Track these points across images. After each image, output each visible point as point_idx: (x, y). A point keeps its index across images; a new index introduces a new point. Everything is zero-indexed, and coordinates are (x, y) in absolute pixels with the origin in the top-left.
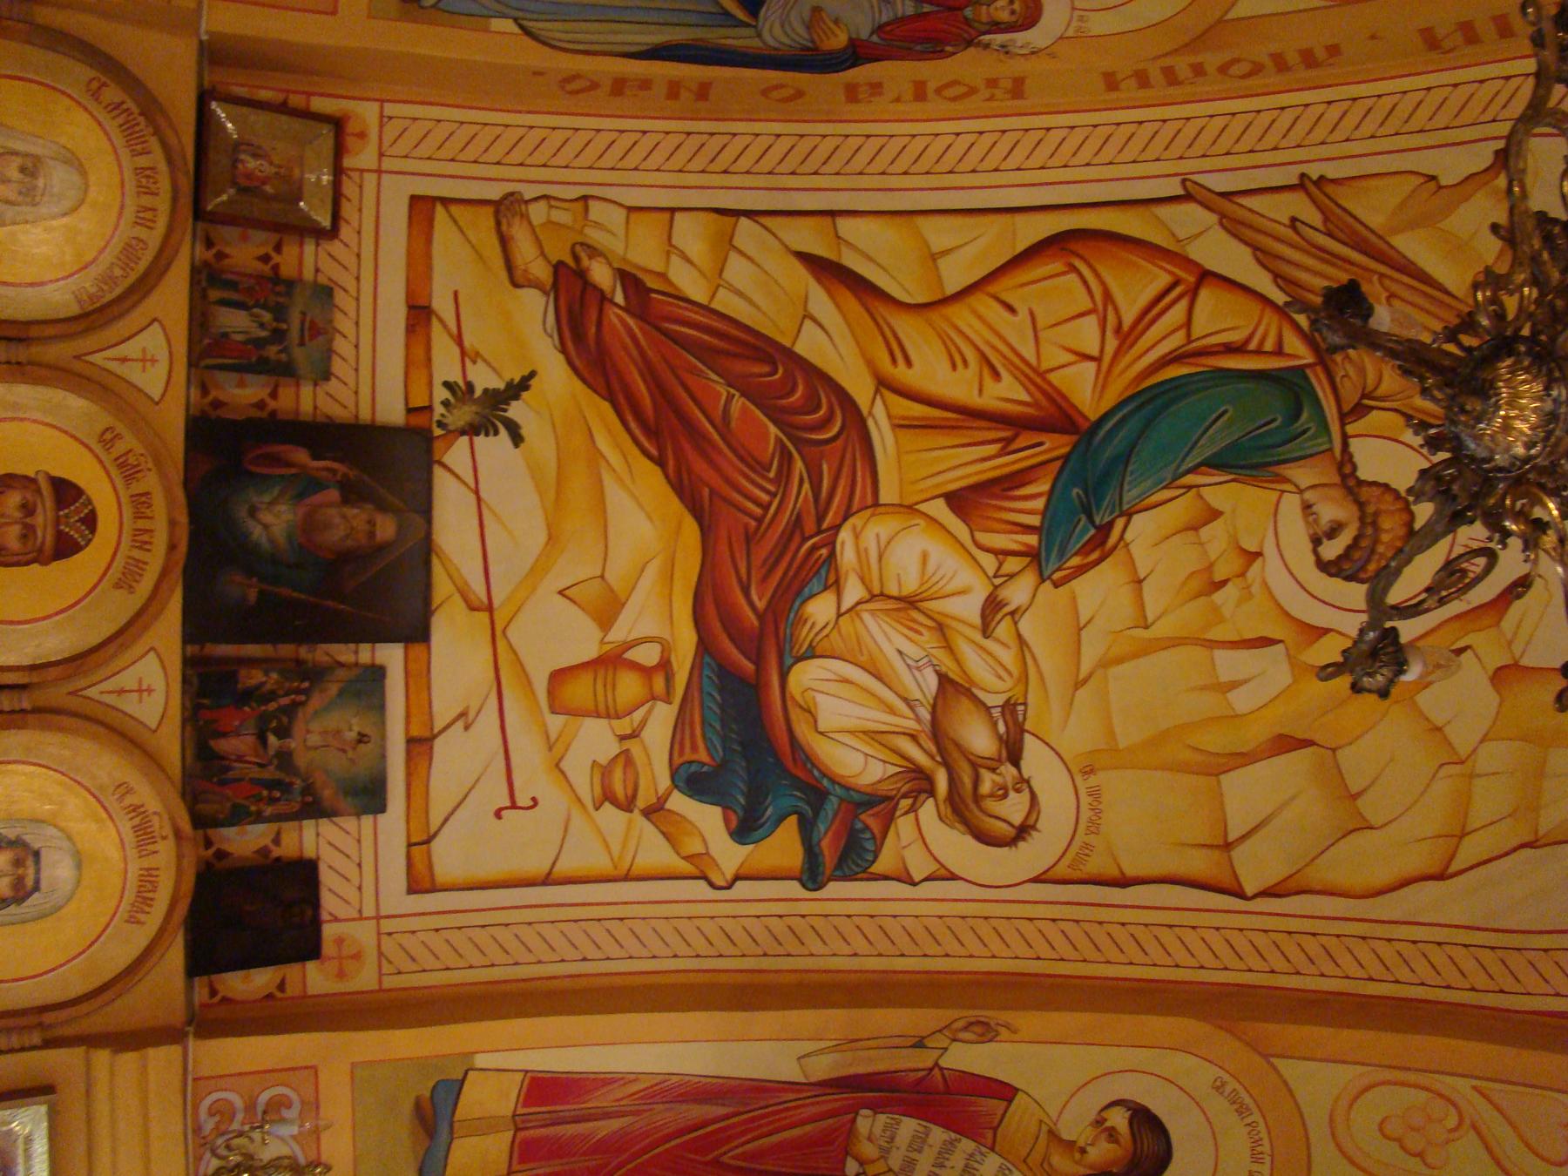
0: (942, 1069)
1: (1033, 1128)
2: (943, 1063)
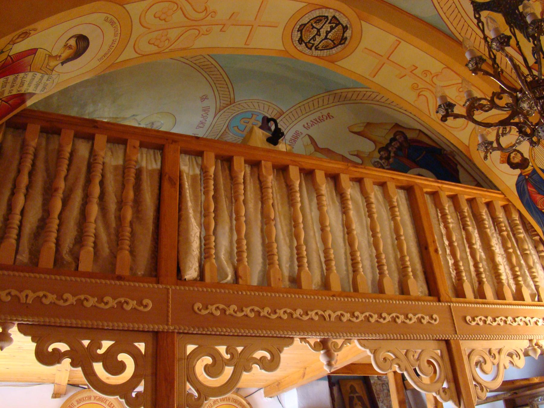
0: (10, 56)
1: (44, 56)
2: (10, 55)
